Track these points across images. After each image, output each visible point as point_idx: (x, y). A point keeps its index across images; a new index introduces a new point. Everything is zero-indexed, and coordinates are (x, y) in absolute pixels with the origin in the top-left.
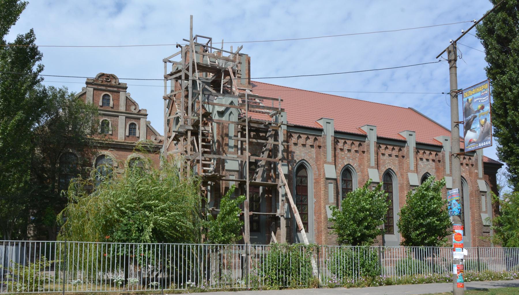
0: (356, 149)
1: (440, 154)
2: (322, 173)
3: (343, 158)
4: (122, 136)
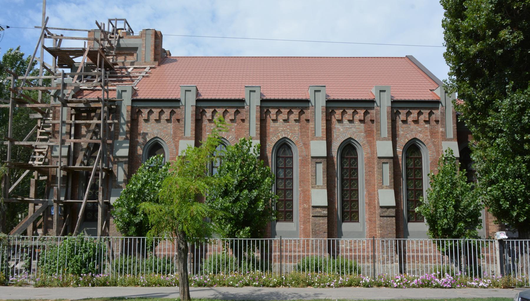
0: (231, 118)
1: (372, 112)
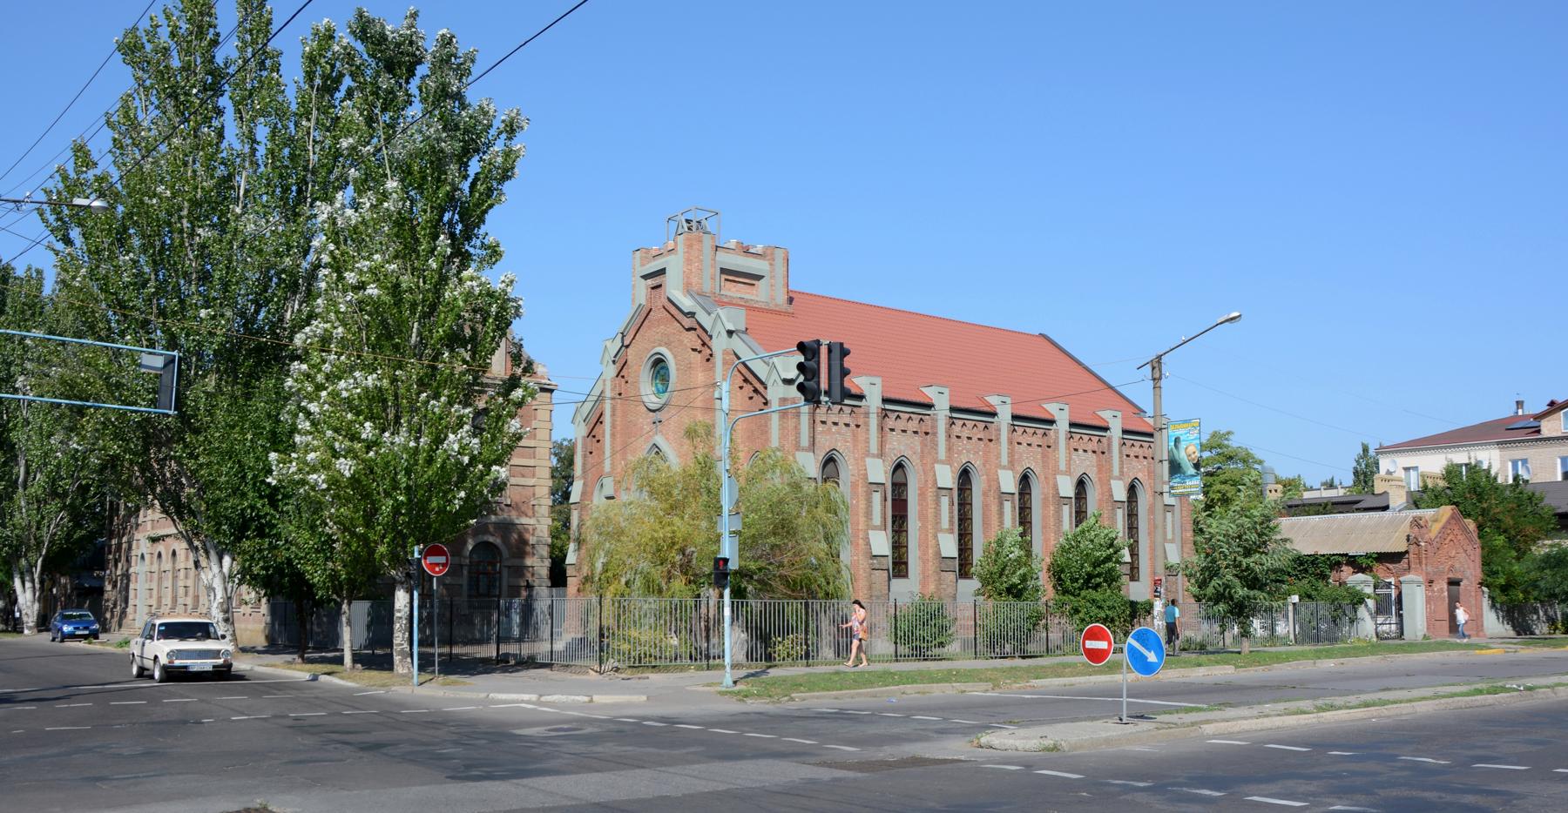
2: (930, 479)
3: (960, 453)
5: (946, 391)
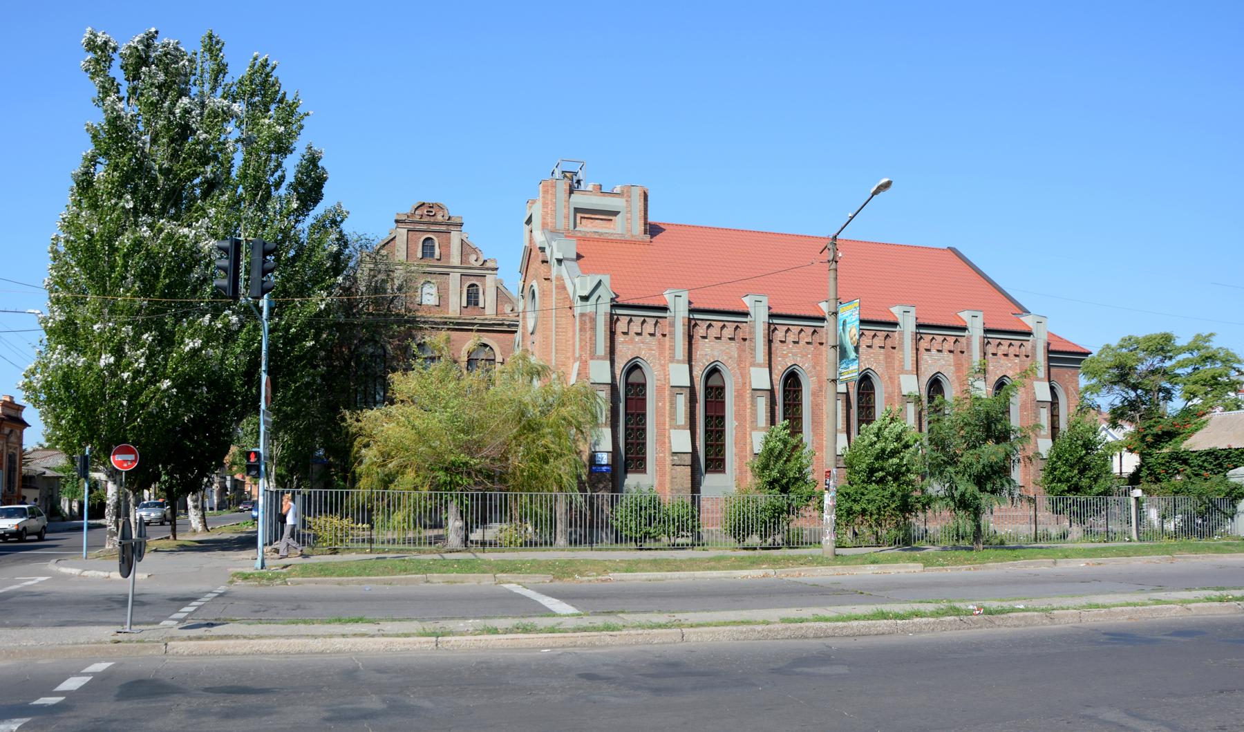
4: (455, 307)
5: (980, 314)
